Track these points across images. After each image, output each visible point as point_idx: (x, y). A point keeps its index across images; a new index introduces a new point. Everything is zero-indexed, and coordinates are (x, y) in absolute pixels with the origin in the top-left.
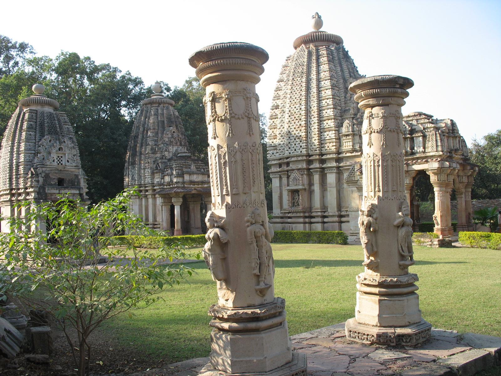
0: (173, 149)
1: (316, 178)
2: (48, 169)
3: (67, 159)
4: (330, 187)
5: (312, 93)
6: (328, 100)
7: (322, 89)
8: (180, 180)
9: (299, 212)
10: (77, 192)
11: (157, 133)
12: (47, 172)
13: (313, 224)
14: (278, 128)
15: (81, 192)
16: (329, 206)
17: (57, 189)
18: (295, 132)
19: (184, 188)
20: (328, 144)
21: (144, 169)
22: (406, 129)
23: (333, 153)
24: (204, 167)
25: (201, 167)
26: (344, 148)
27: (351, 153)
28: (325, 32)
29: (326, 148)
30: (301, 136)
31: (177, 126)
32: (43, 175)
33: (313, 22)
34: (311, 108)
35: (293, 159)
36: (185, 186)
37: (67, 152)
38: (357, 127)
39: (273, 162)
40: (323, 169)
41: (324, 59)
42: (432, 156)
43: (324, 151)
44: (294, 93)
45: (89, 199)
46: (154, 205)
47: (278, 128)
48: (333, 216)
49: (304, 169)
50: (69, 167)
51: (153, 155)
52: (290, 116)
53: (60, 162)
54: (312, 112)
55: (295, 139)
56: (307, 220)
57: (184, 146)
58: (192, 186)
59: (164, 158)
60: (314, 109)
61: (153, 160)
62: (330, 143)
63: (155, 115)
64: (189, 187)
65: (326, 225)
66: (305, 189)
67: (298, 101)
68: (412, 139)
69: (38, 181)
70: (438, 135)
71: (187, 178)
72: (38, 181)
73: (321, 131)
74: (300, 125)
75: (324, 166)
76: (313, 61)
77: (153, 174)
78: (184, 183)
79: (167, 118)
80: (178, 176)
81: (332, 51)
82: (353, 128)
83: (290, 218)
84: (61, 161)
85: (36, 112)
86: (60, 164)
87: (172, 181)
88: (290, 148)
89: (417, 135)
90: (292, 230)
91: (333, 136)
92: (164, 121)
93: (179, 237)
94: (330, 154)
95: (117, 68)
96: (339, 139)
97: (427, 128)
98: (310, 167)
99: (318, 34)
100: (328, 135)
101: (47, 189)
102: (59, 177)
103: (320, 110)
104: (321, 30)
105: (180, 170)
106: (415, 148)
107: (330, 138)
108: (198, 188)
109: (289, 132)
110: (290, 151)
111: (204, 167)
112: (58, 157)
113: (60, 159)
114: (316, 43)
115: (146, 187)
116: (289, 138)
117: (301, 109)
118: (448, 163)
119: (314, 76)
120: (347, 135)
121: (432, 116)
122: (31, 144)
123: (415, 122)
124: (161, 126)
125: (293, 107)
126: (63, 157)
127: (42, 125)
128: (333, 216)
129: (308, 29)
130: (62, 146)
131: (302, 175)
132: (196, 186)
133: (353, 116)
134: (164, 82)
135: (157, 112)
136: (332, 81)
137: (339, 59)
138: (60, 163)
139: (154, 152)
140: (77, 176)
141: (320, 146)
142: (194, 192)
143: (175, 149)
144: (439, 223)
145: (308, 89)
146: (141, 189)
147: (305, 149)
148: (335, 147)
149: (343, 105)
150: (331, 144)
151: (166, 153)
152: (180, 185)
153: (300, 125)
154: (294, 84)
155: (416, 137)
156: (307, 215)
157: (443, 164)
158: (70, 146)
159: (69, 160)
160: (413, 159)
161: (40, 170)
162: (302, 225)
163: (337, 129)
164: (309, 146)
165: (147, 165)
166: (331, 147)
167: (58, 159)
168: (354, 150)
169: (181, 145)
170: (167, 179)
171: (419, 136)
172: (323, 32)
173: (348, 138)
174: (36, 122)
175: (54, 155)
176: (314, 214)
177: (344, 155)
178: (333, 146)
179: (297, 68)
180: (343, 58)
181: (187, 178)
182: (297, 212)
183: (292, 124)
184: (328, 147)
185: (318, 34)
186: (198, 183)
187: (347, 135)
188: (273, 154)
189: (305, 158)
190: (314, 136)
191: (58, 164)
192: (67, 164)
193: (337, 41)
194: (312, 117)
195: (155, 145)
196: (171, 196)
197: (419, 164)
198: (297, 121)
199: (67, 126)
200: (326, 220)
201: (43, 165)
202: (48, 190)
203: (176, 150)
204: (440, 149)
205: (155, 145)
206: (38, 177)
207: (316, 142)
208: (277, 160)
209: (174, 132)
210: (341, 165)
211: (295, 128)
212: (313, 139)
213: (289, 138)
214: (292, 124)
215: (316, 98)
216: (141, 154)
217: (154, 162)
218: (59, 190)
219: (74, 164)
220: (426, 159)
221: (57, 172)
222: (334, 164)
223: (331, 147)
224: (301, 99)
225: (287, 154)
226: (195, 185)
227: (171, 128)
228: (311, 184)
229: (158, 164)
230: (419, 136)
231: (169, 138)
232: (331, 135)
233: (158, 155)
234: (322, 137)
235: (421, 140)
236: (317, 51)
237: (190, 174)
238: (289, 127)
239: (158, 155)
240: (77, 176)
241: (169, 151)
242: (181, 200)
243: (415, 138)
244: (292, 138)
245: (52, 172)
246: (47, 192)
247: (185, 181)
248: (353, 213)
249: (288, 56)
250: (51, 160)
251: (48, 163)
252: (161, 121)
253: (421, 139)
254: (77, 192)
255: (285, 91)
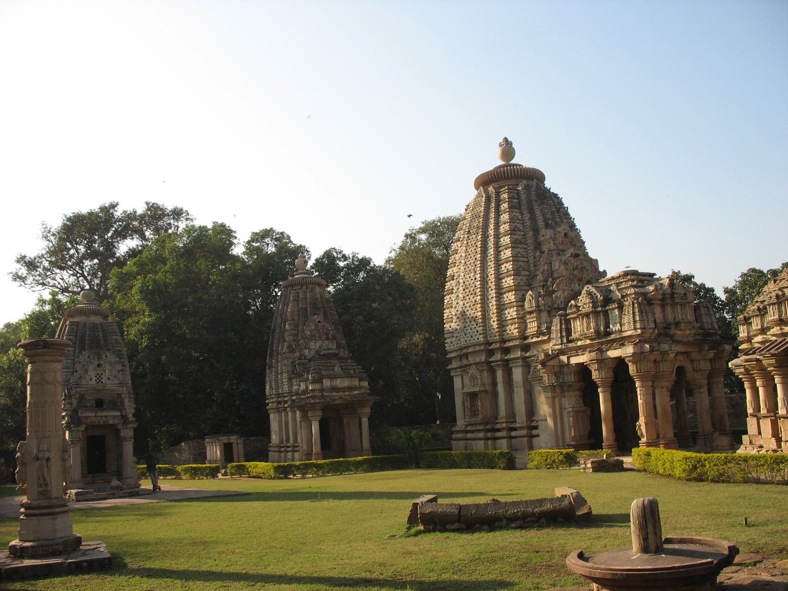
0: (315, 345)
1: (499, 374)
2: (83, 389)
3: (107, 376)
4: (517, 387)
5: (489, 255)
6: (508, 264)
7: (501, 248)
8: (317, 386)
9: (478, 424)
10: (119, 414)
11: (297, 325)
12: (82, 393)
13: (498, 441)
14: (454, 306)
15: (124, 414)
16: (517, 414)
17: (92, 412)
18: (470, 313)
19: (323, 396)
20: (510, 326)
21: (282, 373)
22: (597, 299)
23: (516, 339)
24: (355, 367)
25: (350, 368)
26: (529, 331)
27: (538, 337)
28: (520, 165)
29: (508, 331)
30: (476, 317)
31: (325, 313)
32: (77, 396)
33: (498, 151)
34: (488, 276)
35: (471, 350)
36: (325, 394)
37: (108, 368)
38: (543, 299)
39: (453, 355)
40: (508, 361)
41: (505, 206)
42: (630, 337)
43: (506, 337)
44: (469, 257)
45: (136, 421)
46: (294, 420)
47: (454, 306)
48: (522, 428)
49: (482, 363)
50: (110, 386)
51: (290, 354)
52: (464, 290)
53: (100, 381)
54: (489, 282)
55: (471, 322)
56: (489, 435)
57: (332, 339)
58: (334, 394)
59: (303, 358)
60: (492, 278)
61: (291, 361)
62: (512, 324)
63: (294, 300)
64: (331, 396)
65: (514, 441)
66: (486, 391)
67: (473, 268)
68: (606, 314)
69: (71, 404)
70: (636, 305)
71: (327, 383)
72: (71, 404)
73: (501, 308)
74: (476, 301)
75: (507, 357)
76: (491, 209)
77: (290, 379)
78: (322, 390)
79: (310, 304)
80: (314, 381)
81: (518, 192)
82: (537, 302)
83: (472, 432)
84: (102, 378)
85: (77, 324)
86: (100, 383)
87: (307, 388)
88: (465, 334)
89: (611, 307)
90: (472, 450)
91: (514, 315)
92: (306, 309)
93: (320, 462)
94: (513, 340)
95: (283, 232)
96: (522, 320)
97: (627, 295)
98: (490, 360)
99: (507, 169)
100: (509, 313)
101: (80, 412)
102: (97, 397)
103: (499, 278)
104: (513, 162)
105: (317, 373)
106: (611, 326)
107: (512, 318)
108: (345, 395)
109: (464, 312)
110: (466, 339)
111: (355, 367)
112: (98, 374)
113: (100, 376)
114: (500, 183)
115: (284, 397)
116: (465, 320)
117: (475, 279)
118: (647, 346)
119: (491, 232)
120: (531, 313)
121: (654, 274)
122: (68, 361)
123: (615, 287)
124: (304, 315)
125: (468, 276)
126: (104, 374)
127: (82, 339)
128: (522, 428)
129: (494, 161)
130: (101, 362)
131: (482, 371)
132: (341, 393)
133: (542, 284)
134: (337, 248)
135: (298, 296)
136: (514, 236)
137: (530, 202)
138: (99, 381)
139: (293, 351)
140: (119, 395)
141: (500, 330)
142: (338, 402)
143: (318, 344)
144: (645, 434)
145: (484, 250)
146: (280, 399)
147: (482, 335)
148: (517, 330)
149: (532, 269)
150: (513, 327)
151: (306, 352)
152: (317, 394)
153: (476, 301)
154: (469, 244)
155: (611, 309)
156: (489, 427)
157: (642, 347)
158: (113, 360)
159: (110, 377)
160: (609, 342)
161: (73, 391)
162: (482, 442)
163: (520, 304)
164: (488, 331)
165: (284, 368)
166: (513, 330)
167: (98, 377)
168: (539, 333)
169: (327, 339)
170: (303, 386)
171: (614, 309)
172: (516, 165)
173: (532, 316)
174: (76, 336)
175: (92, 374)
176: (498, 426)
177: (530, 340)
178: (515, 328)
179: (473, 221)
180: (535, 201)
181: (327, 383)
182: (476, 424)
183: (466, 301)
184: (510, 330)
185: (507, 169)
186: (343, 389)
187: (531, 313)
188: (451, 343)
189: (482, 347)
190: (492, 316)
191: (98, 383)
192: (108, 382)
193: (535, 177)
194: (490, 289)
195: (294, 341)
196: (306, 409)
197: (615, 349)
198: (472, 296)
199: (115, 337)
200: (513, 434)
201: (77, 385)
202: (81, 413)
203: (321, 347)
204: (638, 325)
205: (294, 341)
206: (71, 399)
207: (495, 325)
208: (456, 351)
209: (319, 322)
210: (528, 355)
211: (470, 306)
212: (492, 320)
213: (465, 320)
214: (466, 301)
215: (493, 262)
216: (278, 353)
217: (292, 363)
218: (96, 413)
219: (117, 382)
220: (622, 342)
221: (94, 392)
222: (518, 354)
223: (513, 330)
224: (476, 265)
225: (463, 343)
226: (339, 392)
227: (316, 316)
228: (494, 384)
229: (295, 366)
230: (614, 309)
231: (311, 331)
232: (511, 313)
233: (297, 354)
234: (503, 316)
235: (617, 313)
236: (498, 194)
237: (332, 377)
238: (464, 304)
239: (297, 354)
240: (119, 395)
241: (310, 349)
242: (320, 413)
243: (609, 312)
244: (467, 320)
245: (88, 392)
246: (80, 415)
247: (324, 387)
248: (542, 423)
249: (467, 204)
250: (88, 378)
251: (84, 383)
252: (303, 308)
253: (616, 312)
254: (119, 414)
255: (460, 254)
